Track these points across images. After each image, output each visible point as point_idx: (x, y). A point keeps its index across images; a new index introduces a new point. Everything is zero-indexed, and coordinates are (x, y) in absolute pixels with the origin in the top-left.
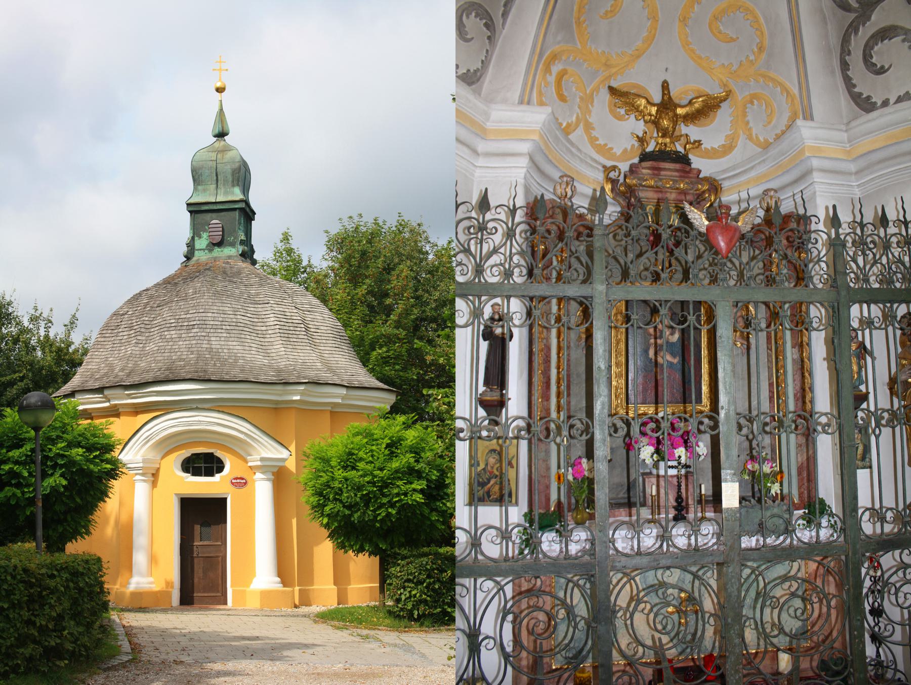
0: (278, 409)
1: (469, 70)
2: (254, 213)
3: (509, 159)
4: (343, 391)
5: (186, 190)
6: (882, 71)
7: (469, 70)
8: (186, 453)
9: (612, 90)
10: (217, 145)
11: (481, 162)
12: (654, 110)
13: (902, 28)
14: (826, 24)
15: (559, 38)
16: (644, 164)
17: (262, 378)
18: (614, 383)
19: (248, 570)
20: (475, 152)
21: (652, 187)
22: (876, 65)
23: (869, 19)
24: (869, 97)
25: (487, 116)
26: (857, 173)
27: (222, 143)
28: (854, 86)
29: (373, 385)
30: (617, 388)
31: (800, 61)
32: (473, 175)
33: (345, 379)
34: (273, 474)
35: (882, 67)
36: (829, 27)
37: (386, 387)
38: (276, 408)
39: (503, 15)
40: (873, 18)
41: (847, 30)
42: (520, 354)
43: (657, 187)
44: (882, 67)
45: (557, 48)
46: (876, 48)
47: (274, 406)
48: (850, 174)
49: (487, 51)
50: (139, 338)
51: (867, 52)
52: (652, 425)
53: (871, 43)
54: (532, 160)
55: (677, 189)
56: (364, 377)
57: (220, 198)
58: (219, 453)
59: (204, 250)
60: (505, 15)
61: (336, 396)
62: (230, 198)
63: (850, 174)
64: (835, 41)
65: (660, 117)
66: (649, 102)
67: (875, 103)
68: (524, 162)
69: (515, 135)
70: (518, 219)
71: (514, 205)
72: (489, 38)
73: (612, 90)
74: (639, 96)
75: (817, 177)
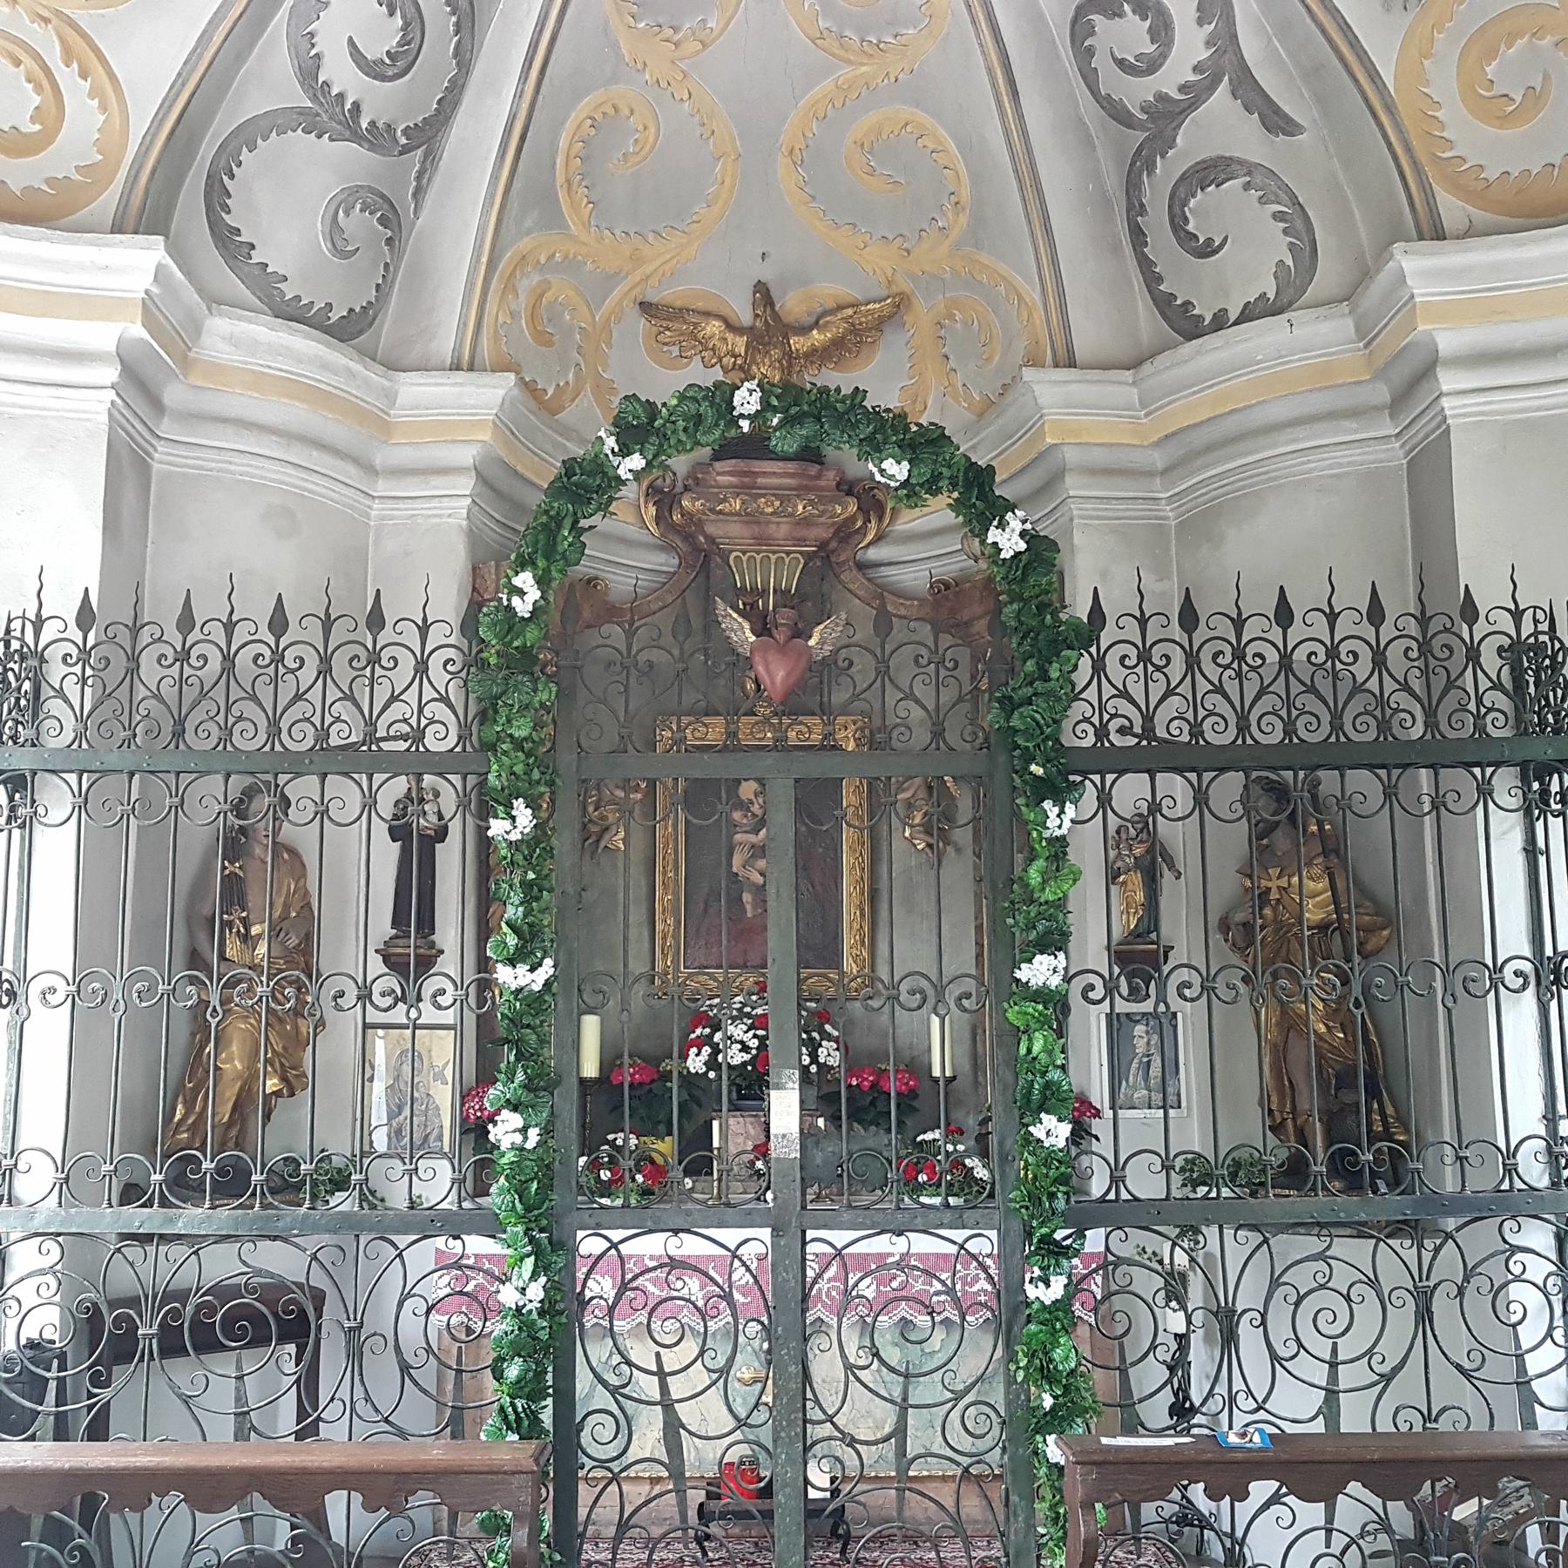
1: (351, 310)
3: (436, 480)
6: (1207, 250)
7: (351, 310)
9: (646, 307)
11: (382, 487)
12: (740, 344)
13: (1241, 162)
14: (1094, 148)
15: (529, 223)
16: (718, 465)
18: (659, 927)
20: (370, 470)
21: (738, 514)
22: (1196, 237)
23: (1171, 144)
24: (1187, 304)
25: (391, 397)
26: (1164, 472)
27: (397, 1524)
28: (1160, 279)
30: (664, 938)
32: (368, 516)
35: (1210, 240)
36: (1100, 152)
39: (414, 195)
40: (1178, 140)
41: (1133, 164)
42: (1493, 247)
43: (747, 514)
44: (1210, 240)
45: (525, 244)
46: (1192, 203)
48: (1151, 474)
49: (387, 265)
51: (1177, 210)
52: (1187, 992)
53: (1182, 193)
54: (482, 478)
55: (791, 515)
60: (419, 193)
63: (1151, 474)
64: (1114, 183)
65: (754, 361)
66: (730, 326)
67: (1201, 318)
68: (466, 484)
69: (444, 430)
70: (436, 636)
71: (425, 619)
72: (389, 241)
73: (646, 307)
74: (708, 314)
75: (1073, 486)
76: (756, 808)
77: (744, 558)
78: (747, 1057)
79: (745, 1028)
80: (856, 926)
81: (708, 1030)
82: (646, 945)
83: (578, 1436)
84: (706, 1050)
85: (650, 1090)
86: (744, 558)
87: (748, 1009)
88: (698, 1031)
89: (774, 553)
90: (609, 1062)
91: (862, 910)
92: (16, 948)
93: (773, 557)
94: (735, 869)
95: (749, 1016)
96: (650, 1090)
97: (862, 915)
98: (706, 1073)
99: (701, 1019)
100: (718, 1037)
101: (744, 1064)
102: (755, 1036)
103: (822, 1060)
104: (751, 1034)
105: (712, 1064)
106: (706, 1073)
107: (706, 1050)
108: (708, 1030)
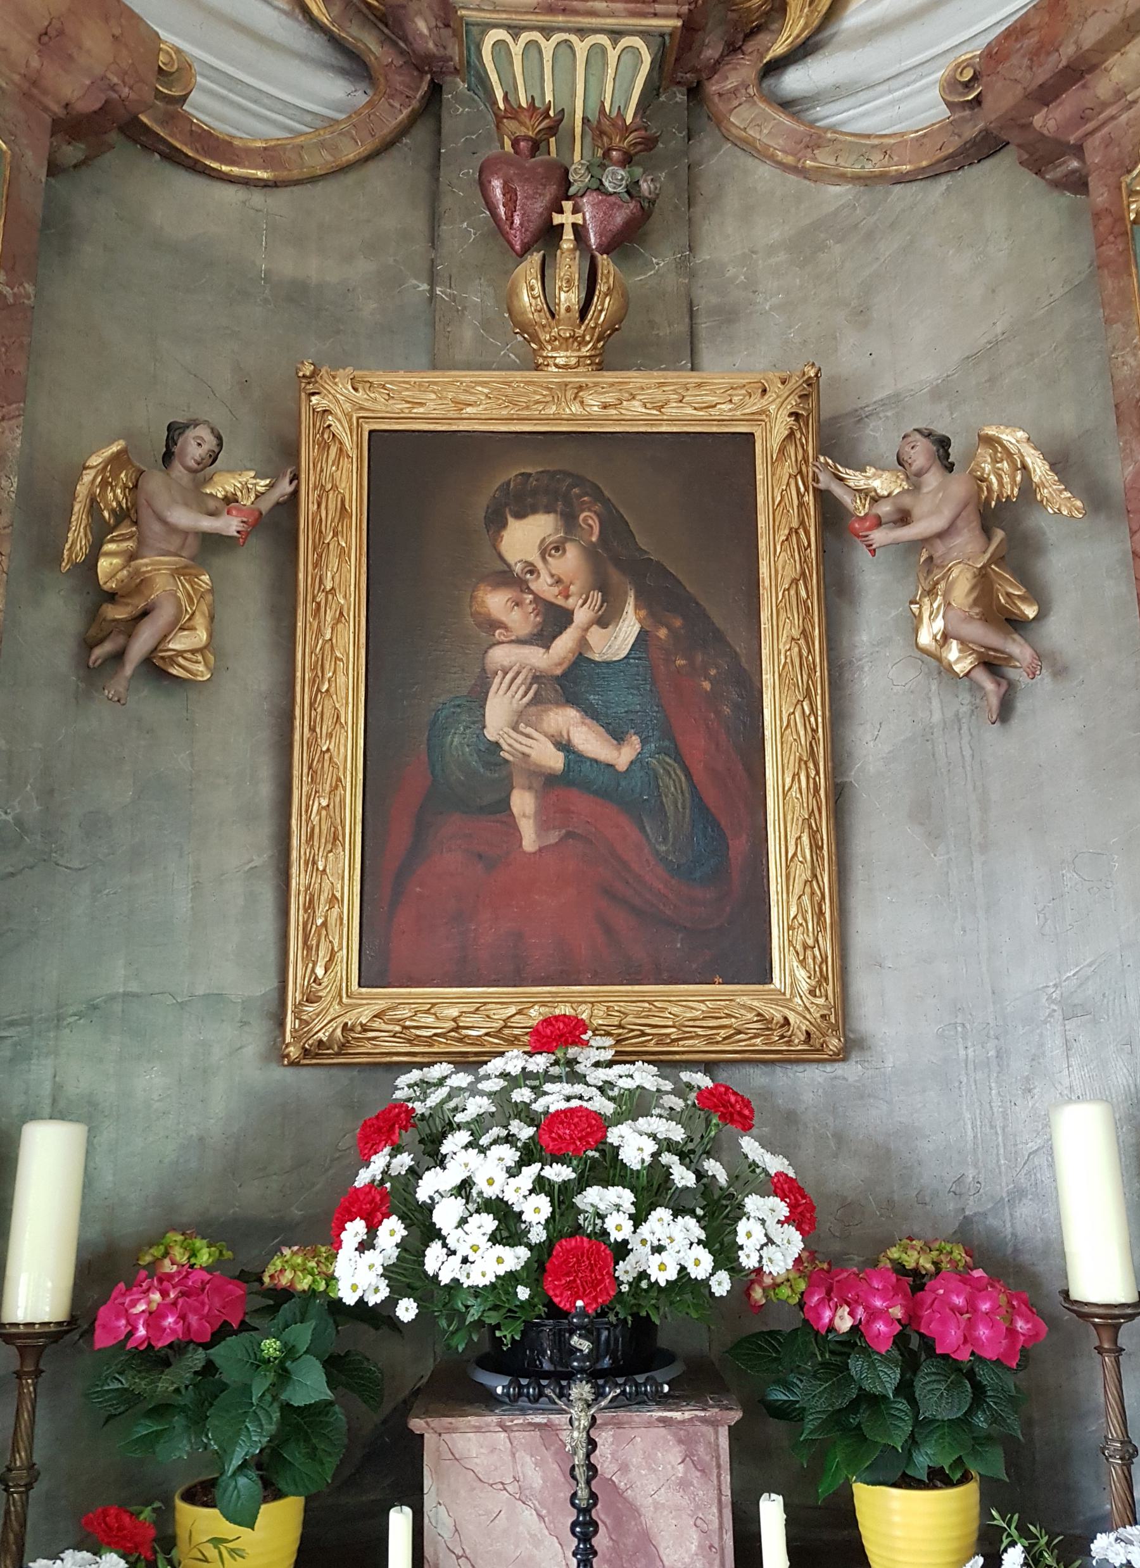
76: (543, 585)
77: (517, 49)
78: (515, 1258)
79: (510, 1155)
80: (802, 873)
81: (405, 1160)
82: (267, 925)
83: (553, 1213)
84: (392, 1231)
85: (210, 1368)
86: (517, 49)
87: (522, 1095)
88: (379, 1161)
89: (582, 32)
90: (101, 1269)
91: (814, 834)
92: (390, 994)
93: (582, 47)
94: (491, 734)
95: (524, 1113)
96: (210, 1368)
97: (816, 847)
98: (391, 1302)
99: (387, 1125)
100: (430, 1184)
101: (511, 1279)
102: (541, 1185)
103: (748, 1260)
104: (530, 1172)
105: (406, 1274)
106: (391, 1302)
107: (392, 1231)
108: (405, 1160)
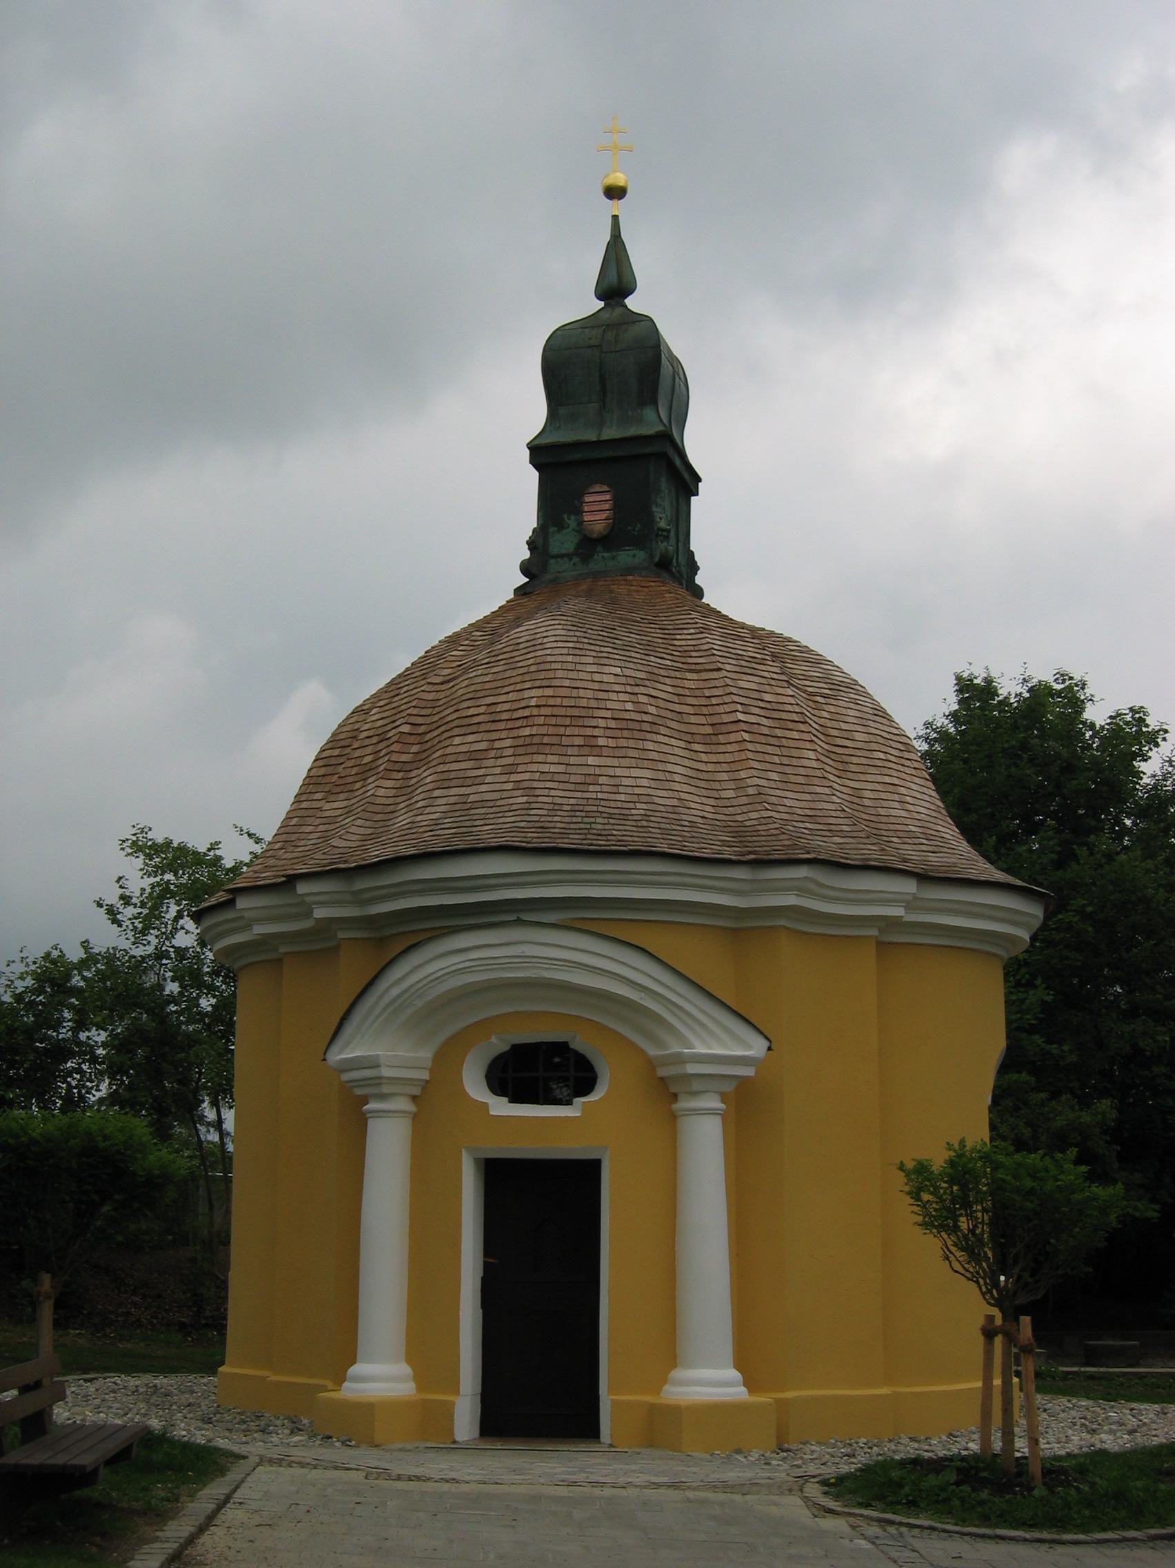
0: (742, 930)
2: (698, 479)
4: (909, 887)
5: (530, 411)
8: (498, 1044)
10: (606, 315)
17: (692, 848)
19: (668, 1352)
27: (618, 311)
29: (973, 874)
31: (676, 1010)
33: (915, 855)
34: (724, 1097)
37: (1001, 876)
38: (735, 931)
47: (729, 924)
50: (394, 757)
56: (959, 853)
57: (610, 433)
58: (580, 1043)
59: (569, 556)
61: (888, 898)
62: (632, 431)
